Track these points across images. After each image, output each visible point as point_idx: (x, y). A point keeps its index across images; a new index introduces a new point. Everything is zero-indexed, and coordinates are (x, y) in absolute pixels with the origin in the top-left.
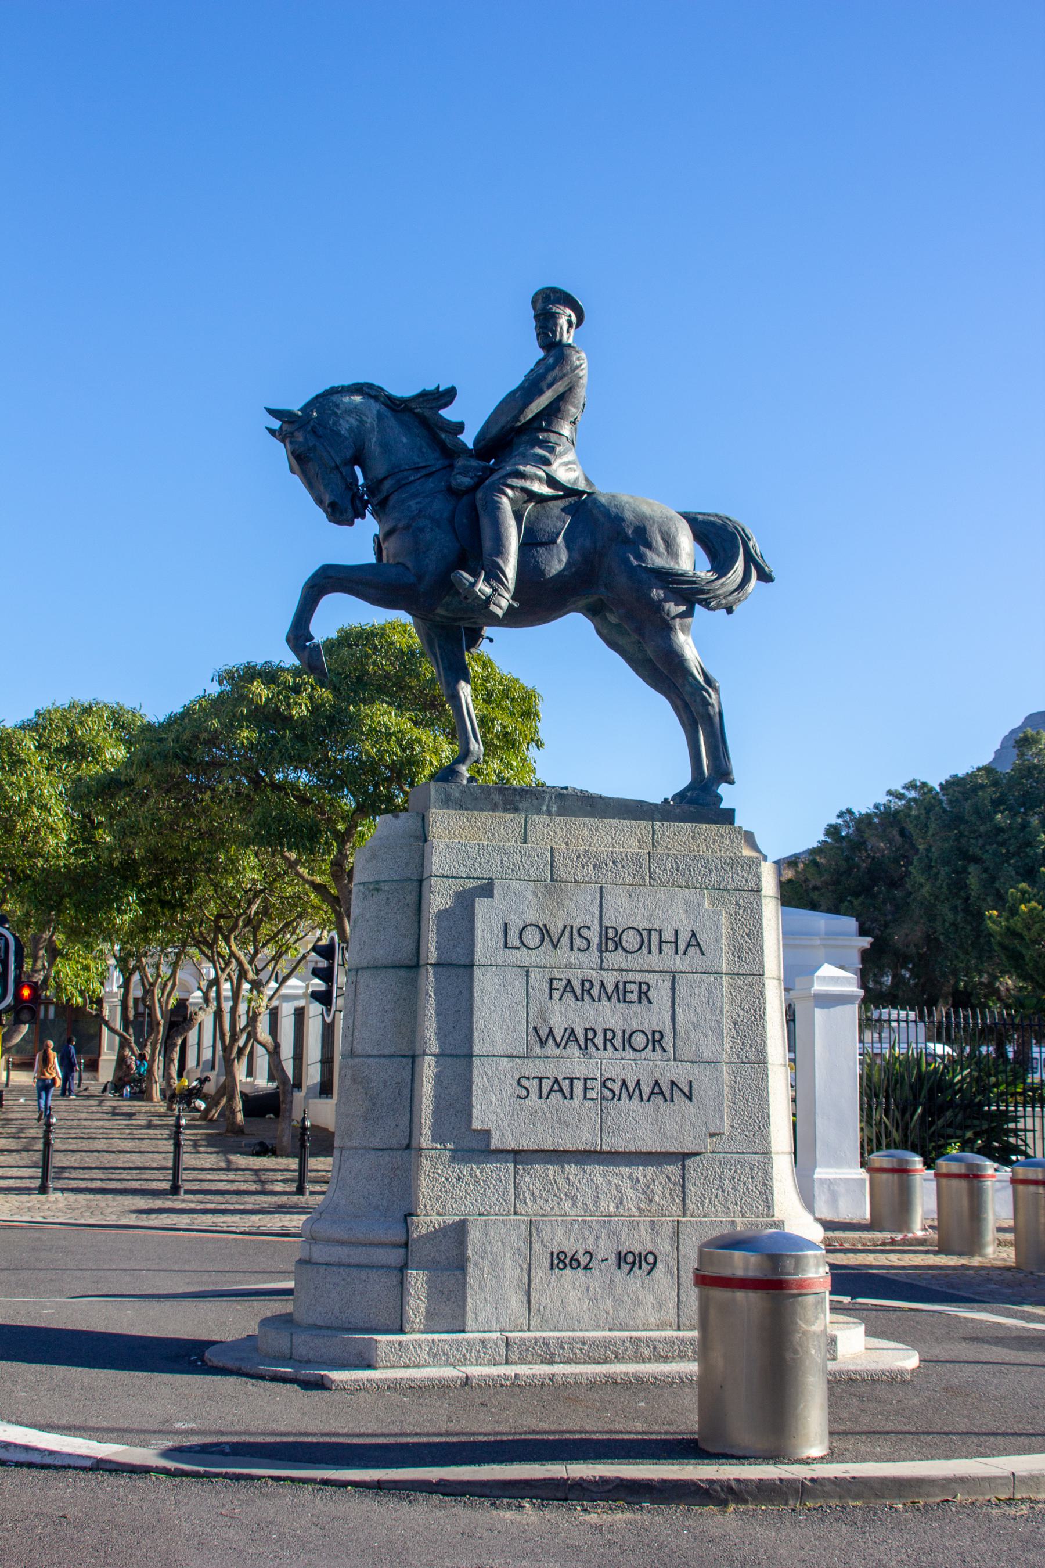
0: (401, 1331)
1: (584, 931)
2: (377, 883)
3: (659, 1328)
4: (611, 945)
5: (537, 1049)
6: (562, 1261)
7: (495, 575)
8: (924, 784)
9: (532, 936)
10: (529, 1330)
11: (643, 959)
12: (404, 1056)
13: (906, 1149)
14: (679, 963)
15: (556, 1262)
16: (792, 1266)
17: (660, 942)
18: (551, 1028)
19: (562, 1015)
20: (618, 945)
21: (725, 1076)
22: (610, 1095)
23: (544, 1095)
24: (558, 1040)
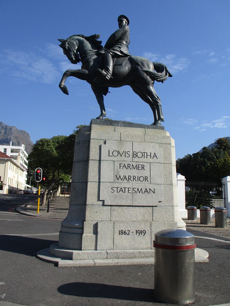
0: (81, 250)
1: (128, 153)
2: (79, 142)
3: (146, 249)
4: (135, 156)
5: (117, 181)
6: (122, 233)
7: (107, 70)
8: (190, 155)
9: (115, 154)
10: (113, 249)
11: (142, 159)
12: (84, 182)
13: (193, 206)
14: (151, 160)
15: (120, 233)
16: (185, 242)
17: (147, 155)
18: (120, 176)
19: (123, 172)
20: (137, 156)
21: (163, 188)
22: (134, 192)
23: (118, 192)
24: (122, 179)
